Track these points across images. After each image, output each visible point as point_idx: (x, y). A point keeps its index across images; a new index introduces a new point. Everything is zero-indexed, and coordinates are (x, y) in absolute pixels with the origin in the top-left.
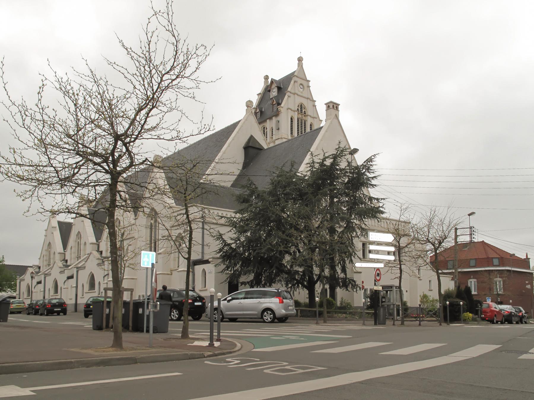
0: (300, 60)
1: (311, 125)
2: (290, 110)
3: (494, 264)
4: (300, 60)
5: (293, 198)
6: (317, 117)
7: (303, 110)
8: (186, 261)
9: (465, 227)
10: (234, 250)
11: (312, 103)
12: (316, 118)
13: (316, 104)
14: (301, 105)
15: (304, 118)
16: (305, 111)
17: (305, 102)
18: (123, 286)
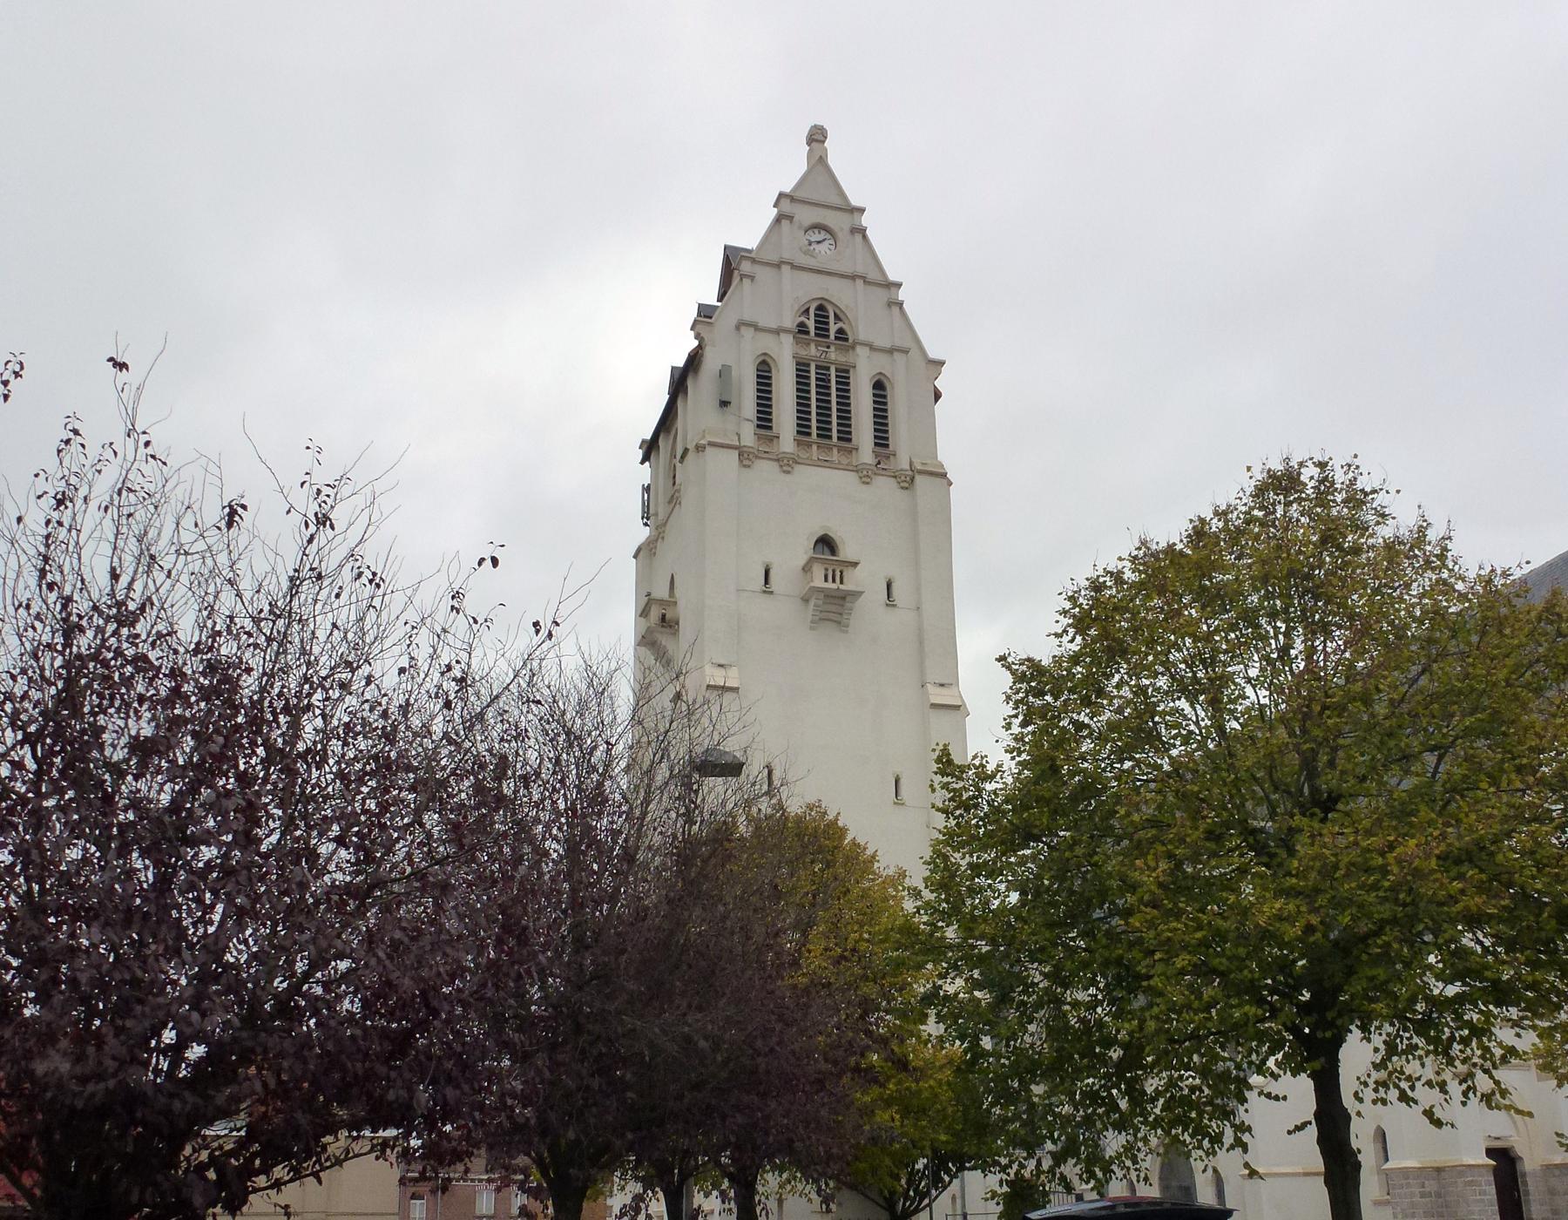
0: (817, 137)
1: (879, 386)
2: (748, 333)
3: (737, 452)
4: (817, 137)
5: (409, 768)
6: (907, 343)
7: (833, 328)
8: (934, 1205)
9: (839, 213)
10: (1471, 930)
11: (881, 295)
12: (906, 352)
13: (902, 295)
14: (821, 308)
15: (833, 355)
16: (840, 331)
17: (840, 294)
18: (1158, 1196)
